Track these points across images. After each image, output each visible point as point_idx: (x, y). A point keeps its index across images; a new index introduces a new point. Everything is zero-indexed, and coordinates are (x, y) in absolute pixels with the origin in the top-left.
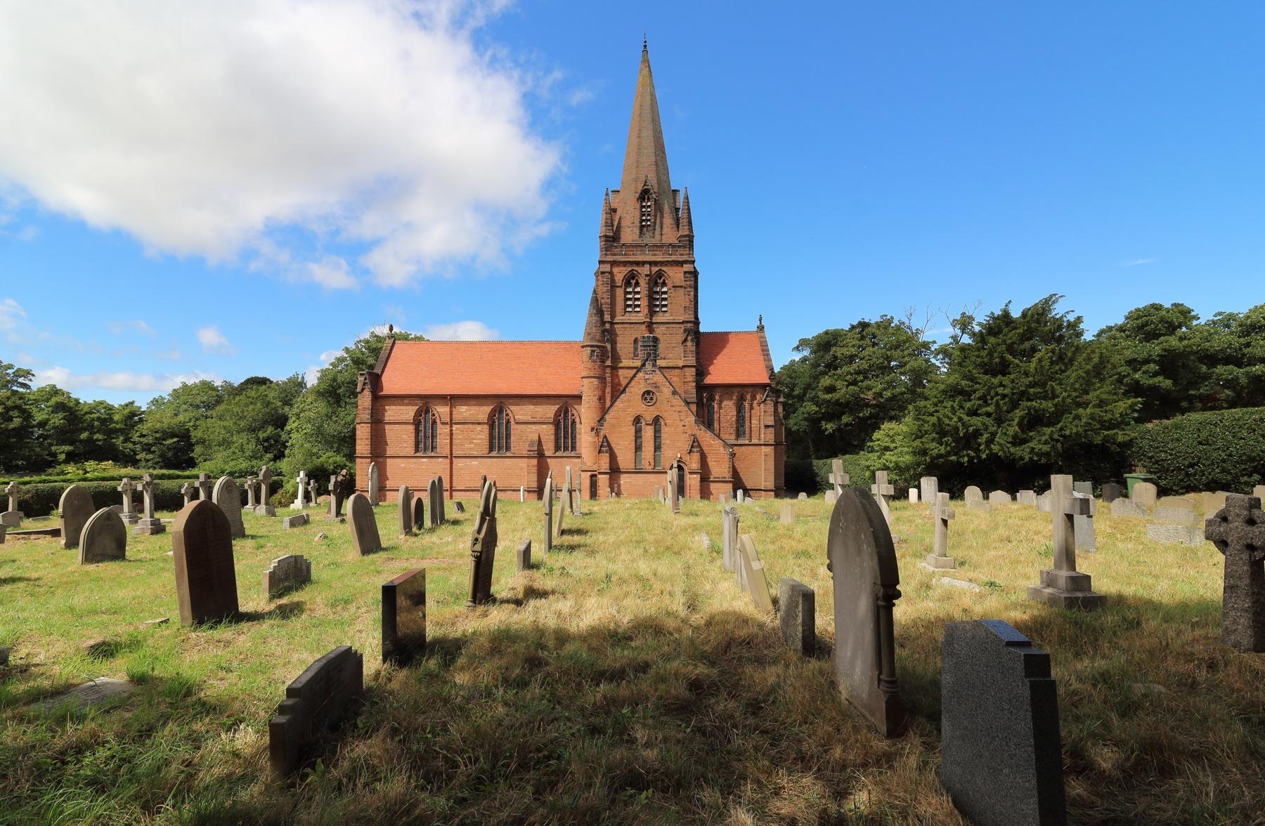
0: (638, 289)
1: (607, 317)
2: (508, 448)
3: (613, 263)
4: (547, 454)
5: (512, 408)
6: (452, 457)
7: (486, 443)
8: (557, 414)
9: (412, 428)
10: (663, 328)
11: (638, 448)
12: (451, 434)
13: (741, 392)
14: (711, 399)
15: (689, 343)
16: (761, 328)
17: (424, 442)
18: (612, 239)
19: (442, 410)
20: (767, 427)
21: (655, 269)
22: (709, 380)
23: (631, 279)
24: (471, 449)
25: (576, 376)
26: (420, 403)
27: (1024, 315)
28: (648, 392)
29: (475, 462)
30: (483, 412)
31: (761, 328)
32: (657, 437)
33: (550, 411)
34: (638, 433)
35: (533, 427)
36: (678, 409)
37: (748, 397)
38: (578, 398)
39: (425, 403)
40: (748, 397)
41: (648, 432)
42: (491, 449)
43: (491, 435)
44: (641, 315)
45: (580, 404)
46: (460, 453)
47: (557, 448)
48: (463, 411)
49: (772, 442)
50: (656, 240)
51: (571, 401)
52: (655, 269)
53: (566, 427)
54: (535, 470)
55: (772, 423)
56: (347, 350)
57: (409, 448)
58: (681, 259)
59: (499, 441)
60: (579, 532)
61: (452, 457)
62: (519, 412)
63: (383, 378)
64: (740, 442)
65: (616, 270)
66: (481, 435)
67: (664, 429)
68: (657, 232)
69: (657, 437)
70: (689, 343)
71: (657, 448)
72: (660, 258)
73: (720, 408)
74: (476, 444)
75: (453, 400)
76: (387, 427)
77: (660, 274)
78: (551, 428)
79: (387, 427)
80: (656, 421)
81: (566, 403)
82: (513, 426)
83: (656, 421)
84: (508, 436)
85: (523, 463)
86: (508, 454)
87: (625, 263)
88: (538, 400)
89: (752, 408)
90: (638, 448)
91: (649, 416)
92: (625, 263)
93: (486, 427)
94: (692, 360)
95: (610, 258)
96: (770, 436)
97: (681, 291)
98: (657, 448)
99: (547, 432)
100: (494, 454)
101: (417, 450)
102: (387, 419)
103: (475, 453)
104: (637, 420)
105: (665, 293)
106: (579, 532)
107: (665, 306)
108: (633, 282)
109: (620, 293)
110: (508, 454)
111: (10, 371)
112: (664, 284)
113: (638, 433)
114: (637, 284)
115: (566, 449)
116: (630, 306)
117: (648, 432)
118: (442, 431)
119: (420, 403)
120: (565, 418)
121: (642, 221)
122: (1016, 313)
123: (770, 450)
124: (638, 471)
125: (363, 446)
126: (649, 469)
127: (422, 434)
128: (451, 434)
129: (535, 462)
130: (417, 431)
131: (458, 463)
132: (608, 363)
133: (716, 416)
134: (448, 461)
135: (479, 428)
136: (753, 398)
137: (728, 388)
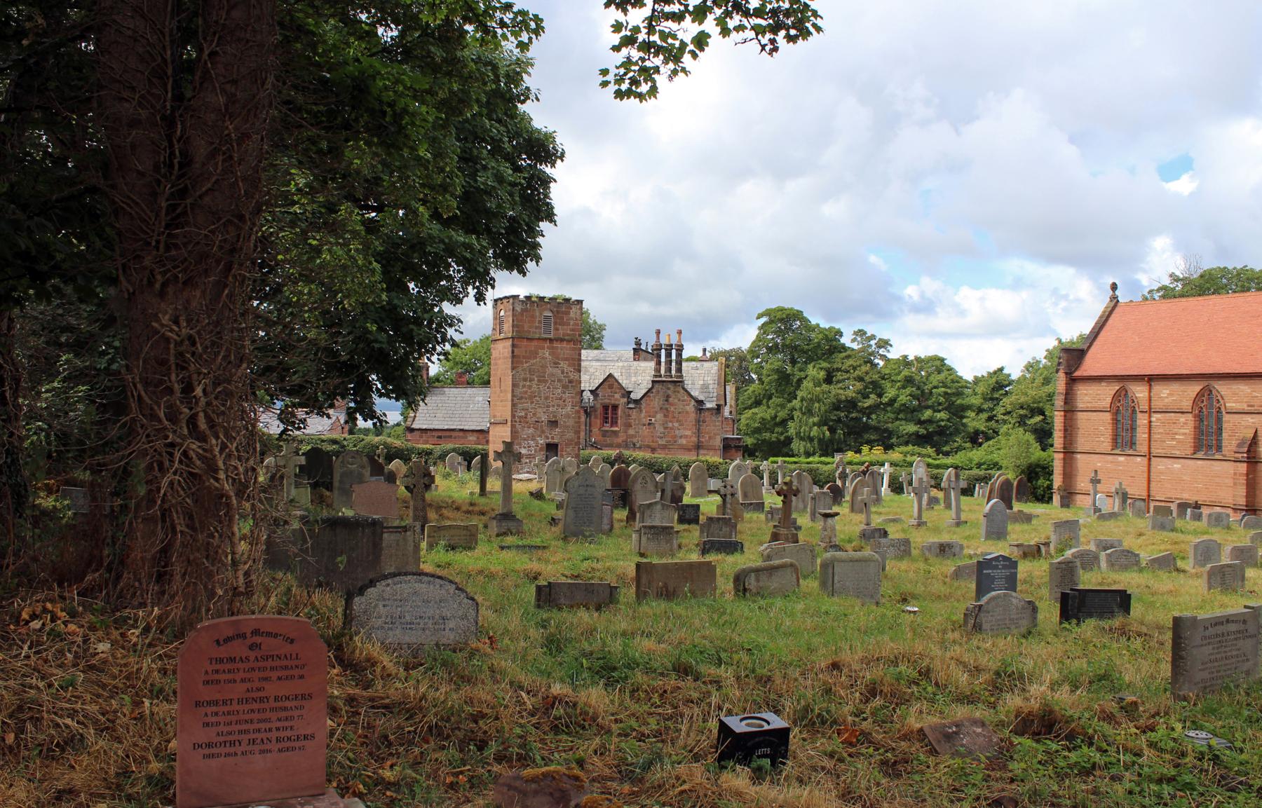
6: (1149, 456)
7: (1190, 441)
9: (1107, 417)
17: (1123, 439)
19: (1139, 392)
24: (1173, 447)
27: (539, 245)
29: (1177, 465)
46: (1161, 452)
48: (1164, 393)
54: (1243, 480)
57: (1105, 443)
60: (209, 756)
61: (1149, 456)
66: (1185, 427)
74: (1179, 441)
75: (1150, 379)
82: (1226, 417)
85: (1229, 467)
103: (1177, 453)
106: (209, 756)
111: (873, 342)
122: (544, 226)
125: (1058, 439)
130: (1115, 421)
131: (1159, 465)
134: (1146, 459)
135: (1182, 418)
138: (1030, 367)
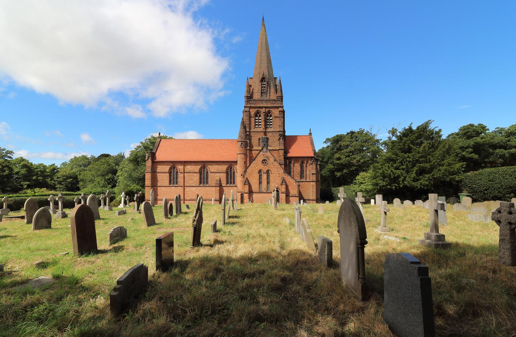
0: (260, 118)
1: (248, 129)
2: (207, 183)
3: (250, 107)
4: (223, 185)
5: (209, 166)
6: (184, 186)
7: (198, 181)
8: (227, 169)
9: (168, 174)
10: (270, 134)
11: (260, 183)
12: (184, 177)
13: (302, 160)
14: (290, 163)
15: (281, 140)
16: (310, 134)
17: (173, 180)
18: (249, 98)
19: (180, 167)
20: (313, 174)
21: (267, 110)
22: (289, 155)
23: (257, 114)
24: (192, 183)
25: (235, 153)
26: (171, 164)
27: (418, 128)
28: (264, 160)
29: (194, 189)
30: (197, 168)
31: (310, 134)
32: (268, 178)
33: (224, 168)
34: (260, 176)
35: (218, 174)
36: (277, 167)
37: (305, 162)
38: (236, 162)
39: (173, 164)
40: (305, 162)
41: (264, 176)
42: (200, 183)
43: (200, 177)
44: (262, 129)
45: (237, 165)
46: (188, 185)
47: (227, 183)
48: (189, 168)
49: (315, 180)
50: (268, 98)
51: (233, 164)
52: (267, 110)
53: (231, 174)
54: (218, 192)
55: (315, 173)
56: (141, 143)
57: (167, 183)
58: (278, 106)
59: (203, 180)
60: (236, 217)
61: (184, 186)
62: (212, 168)
63: (156, 154)
64: (302, 180)
65: (251, 110)
66: (196, 178)
67: (271, 175)
68: (268, 95)
69: (268, 178)
70: (281, 140)
71: (268, 183)
72: (269, 105)
73: (294, 166)
74: (194, 181)
75: (185, 163)
76: (158, 174)
77: (269, 112)
78: (225, 175)
79: (158, 174)
80: (268, 172)
81: (231, 164)
82: (209, 174)
83: (268, 172)
84: (207, 178)
85: (213, 189)
86: (207, 185)
87: (255, 107)
88: (220, 163)
89: (307, 167)
90: (260, 183)
91: (265, 170)
92: (255, 107)
93: (198, 174)
94: (282, 147)
95: (249, 105)
96: (314, 178)
97: (278, 119)
98: (268, 183)
99: (223, 176)
100: (202, 185)
101: (170, 184)
102: (158, 171)
103: (194, 185)
104: (260, 171)
105: (271, 119)
106: (236, 217)
107: (271, 125)
108: (258, 115)
109: (253, 119)
110: (207, 185)
111: (4, 151)
112: (271, 116)
113: (260, 176)
114: (260, 116)
115: (231, 183)
116: (257, 125)
117: (264, 176)
118: (180, 176)
119: (171, 164)
120: (231, 171)
121: (262, 90)
122: (414, 128)
123: (314, 184)
124: (260, 192)
125: (148, 182)
126: (265, 191)
127: (172, 177)
128: (184, 177)
129: (218, 188)
130: (170, 176)
131: (187, 189)
132: (248, 148)
133: (292, 170)
134: (183, 188)
135: (195, 174)
136: (307, 162)
137: (297, 158)
138: (63, 164)
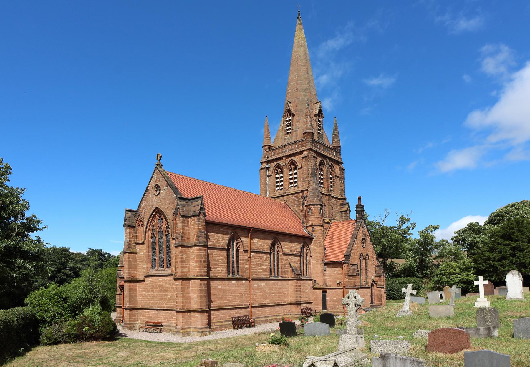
29: (263, 284)
58: (278, 156)
103: (263, 277)
